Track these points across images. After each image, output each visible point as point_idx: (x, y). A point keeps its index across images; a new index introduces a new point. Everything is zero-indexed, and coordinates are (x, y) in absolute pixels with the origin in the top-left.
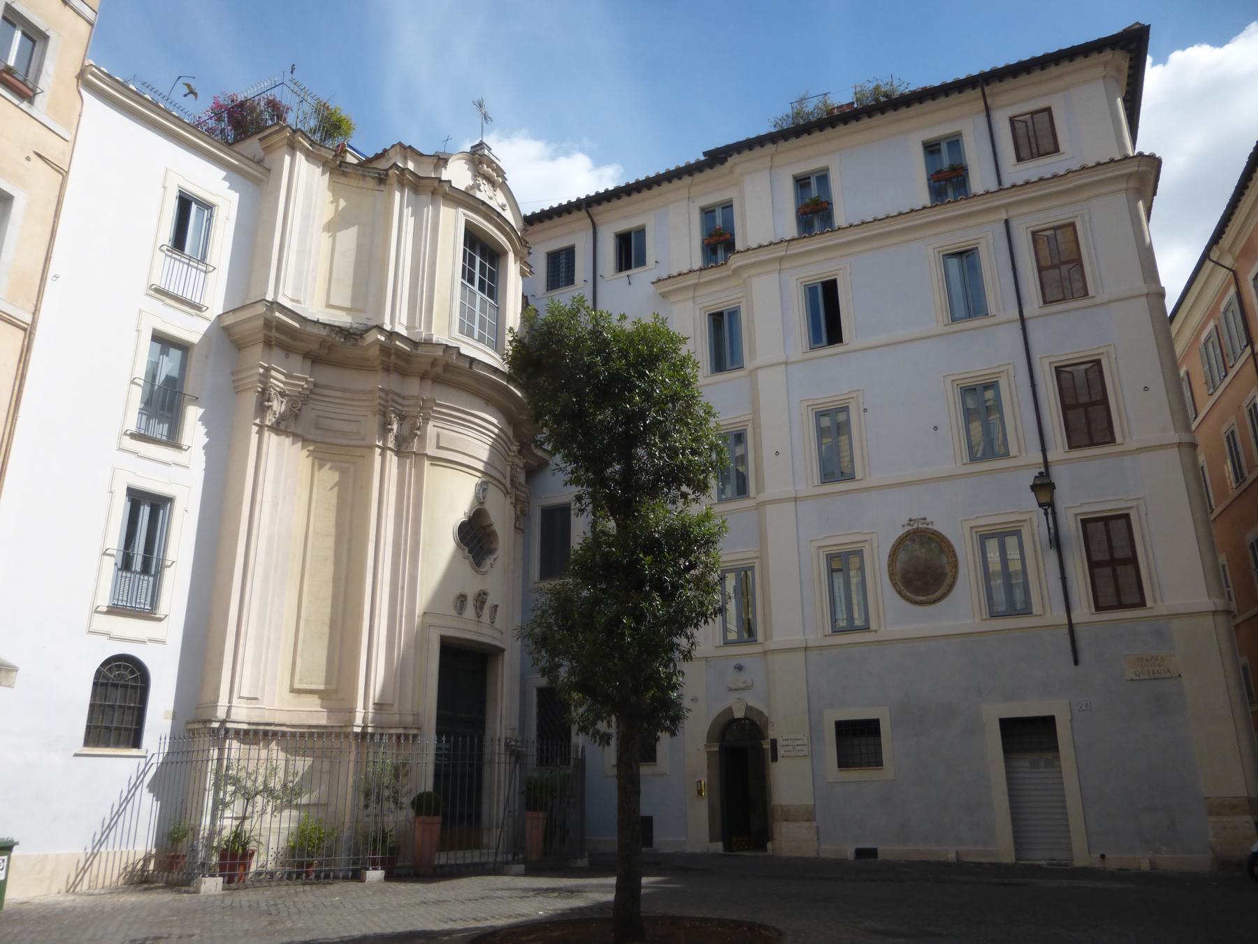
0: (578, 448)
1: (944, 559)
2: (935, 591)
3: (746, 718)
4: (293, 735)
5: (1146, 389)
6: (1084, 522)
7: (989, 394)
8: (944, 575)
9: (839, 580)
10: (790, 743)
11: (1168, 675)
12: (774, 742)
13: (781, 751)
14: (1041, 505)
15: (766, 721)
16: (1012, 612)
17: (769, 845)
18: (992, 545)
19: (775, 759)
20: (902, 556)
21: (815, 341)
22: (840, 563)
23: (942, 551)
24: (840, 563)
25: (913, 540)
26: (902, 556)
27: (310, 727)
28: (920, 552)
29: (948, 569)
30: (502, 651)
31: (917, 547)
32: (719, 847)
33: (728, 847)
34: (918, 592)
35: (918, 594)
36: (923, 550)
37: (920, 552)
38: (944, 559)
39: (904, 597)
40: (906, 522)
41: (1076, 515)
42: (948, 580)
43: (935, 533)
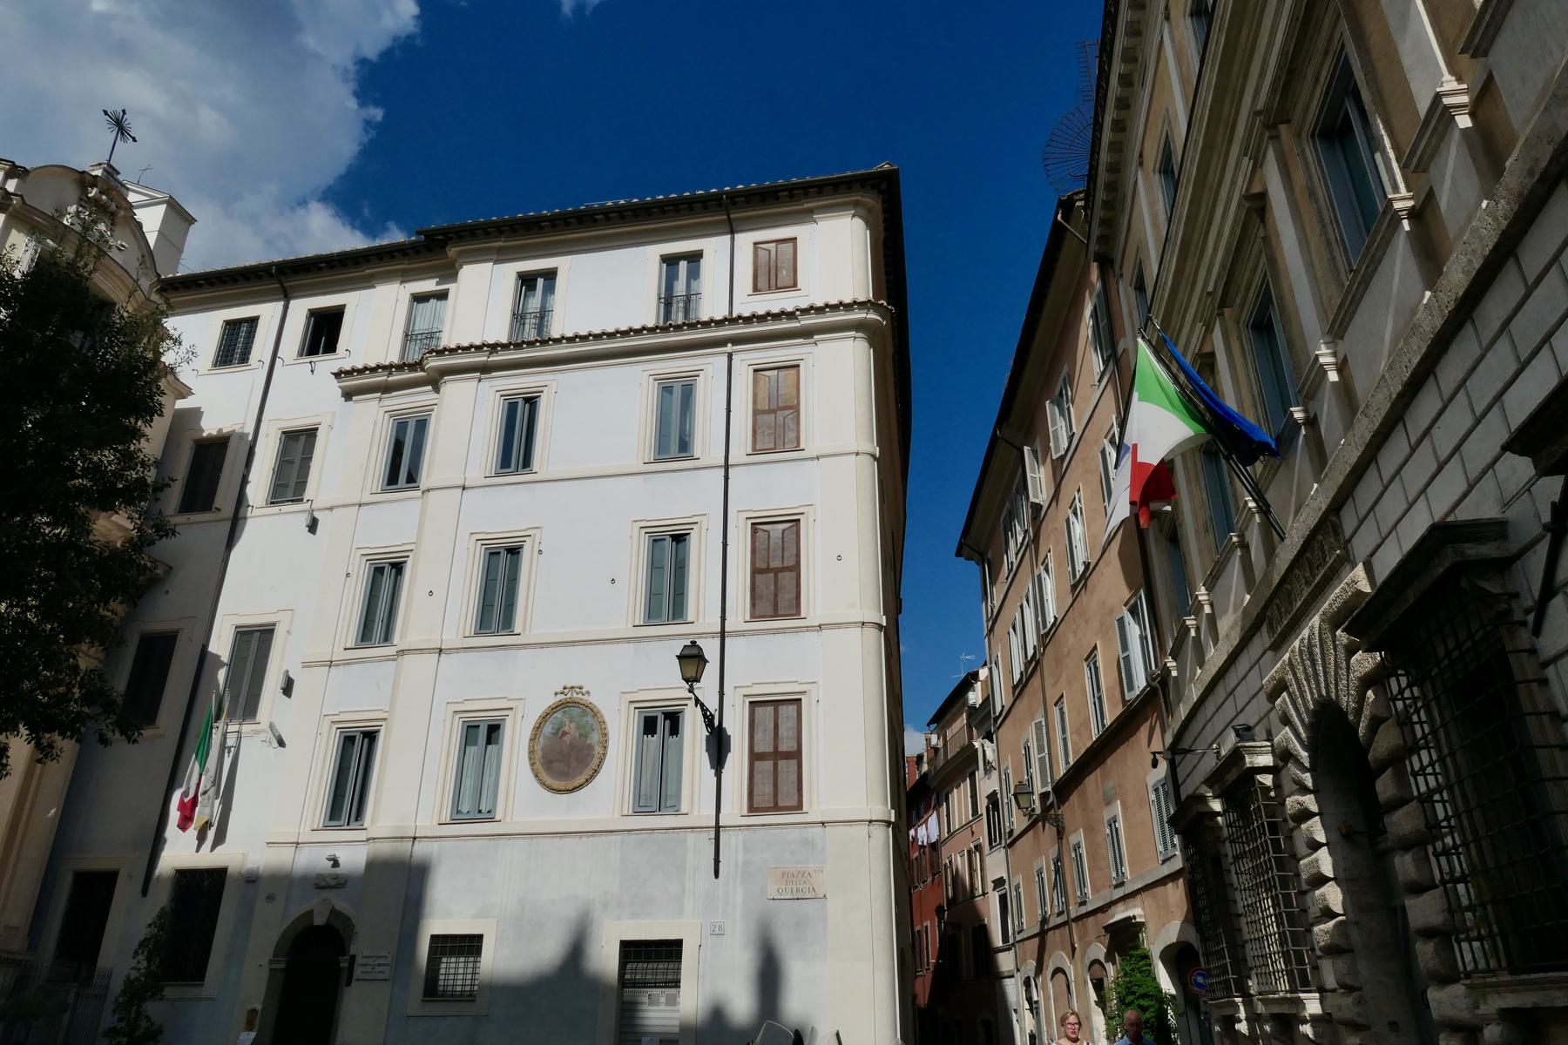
10: (370, 961)
12: (353, 958)
13: (357, 972)
19: (349, 983)
40: (560, 689)
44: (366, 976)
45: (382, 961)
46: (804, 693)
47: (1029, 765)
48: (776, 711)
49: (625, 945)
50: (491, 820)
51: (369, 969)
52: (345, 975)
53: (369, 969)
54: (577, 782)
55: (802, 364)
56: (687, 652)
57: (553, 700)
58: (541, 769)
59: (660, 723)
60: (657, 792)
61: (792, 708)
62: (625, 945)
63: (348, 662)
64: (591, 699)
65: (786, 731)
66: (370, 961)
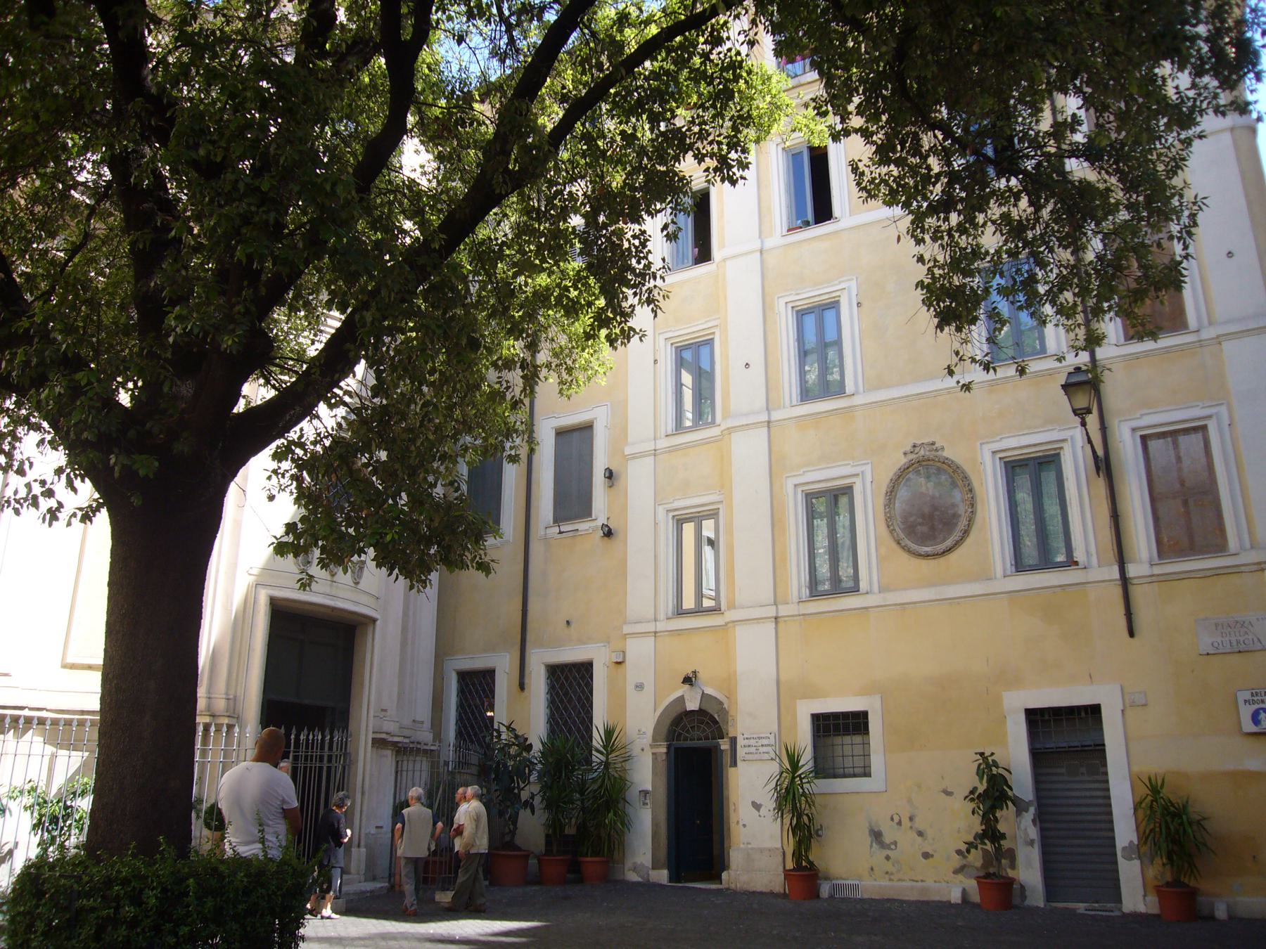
0: (192, 229)
1: (957, 496)
2: (944, 540)
3: (701, 712)
4: (55, 722)
5: (1230, 254)
6: (1144, 439)
7: (1191, 444)
8: (956, 516)
9: (822, 525)
10: (752, 742)
11: (1258, 646)
12: (734, 741)
13: (741, 752)
14: (1075, 412)
15: (724, 712)
16: (1046, 562)
17: (724, 875)
18: (1024, 481)
19: (734, 764)
20: (903, 493)
21: (799, 223)
22: (829, 503)
23: (954, 485)
24: (829, 503)
25: (918, 472)
26: (903, 493)
27: (83, 712)
28: (925, 486)
29: (962, 509)
30: (374, 621)
31: (922, 480)
32: (662, 876)
33: (674, 877)
34: (924, 539)
35: (923, 544)
36: (931, 485)
37: (925, 486)
38: (957, 496)
39: (927, 556)
40: (909, 448)
41: (1134, 430)
42: (962, 524)
43: (946, 462)
44: (750, 757)
45: (765, 742)
46: (1209, 417)
47: (31, 709)
48: (1175, 444)
49: (816, 718)
50: (855, 589)
51: (753, 750)
52: (727, 759)
53: (753, 750)
54: (949, 543)
55: (785, 233)
56: (1074, 379)
57: (903, 461)
58: (902, 535)
59: (1032, 471)
60: (1039, 547)
61: (1196, 438)
62: (816, 718)
63: (672, 450)
64: (946, 454)
65: (1024, 498)
66: (752, 742)
